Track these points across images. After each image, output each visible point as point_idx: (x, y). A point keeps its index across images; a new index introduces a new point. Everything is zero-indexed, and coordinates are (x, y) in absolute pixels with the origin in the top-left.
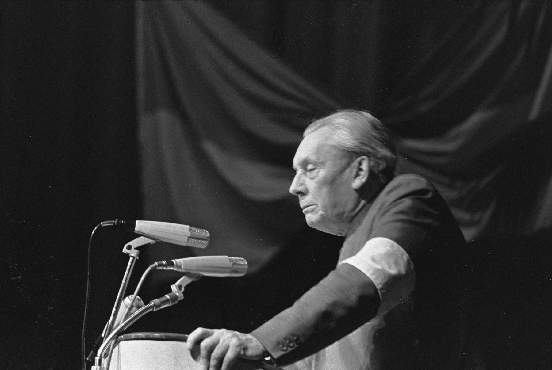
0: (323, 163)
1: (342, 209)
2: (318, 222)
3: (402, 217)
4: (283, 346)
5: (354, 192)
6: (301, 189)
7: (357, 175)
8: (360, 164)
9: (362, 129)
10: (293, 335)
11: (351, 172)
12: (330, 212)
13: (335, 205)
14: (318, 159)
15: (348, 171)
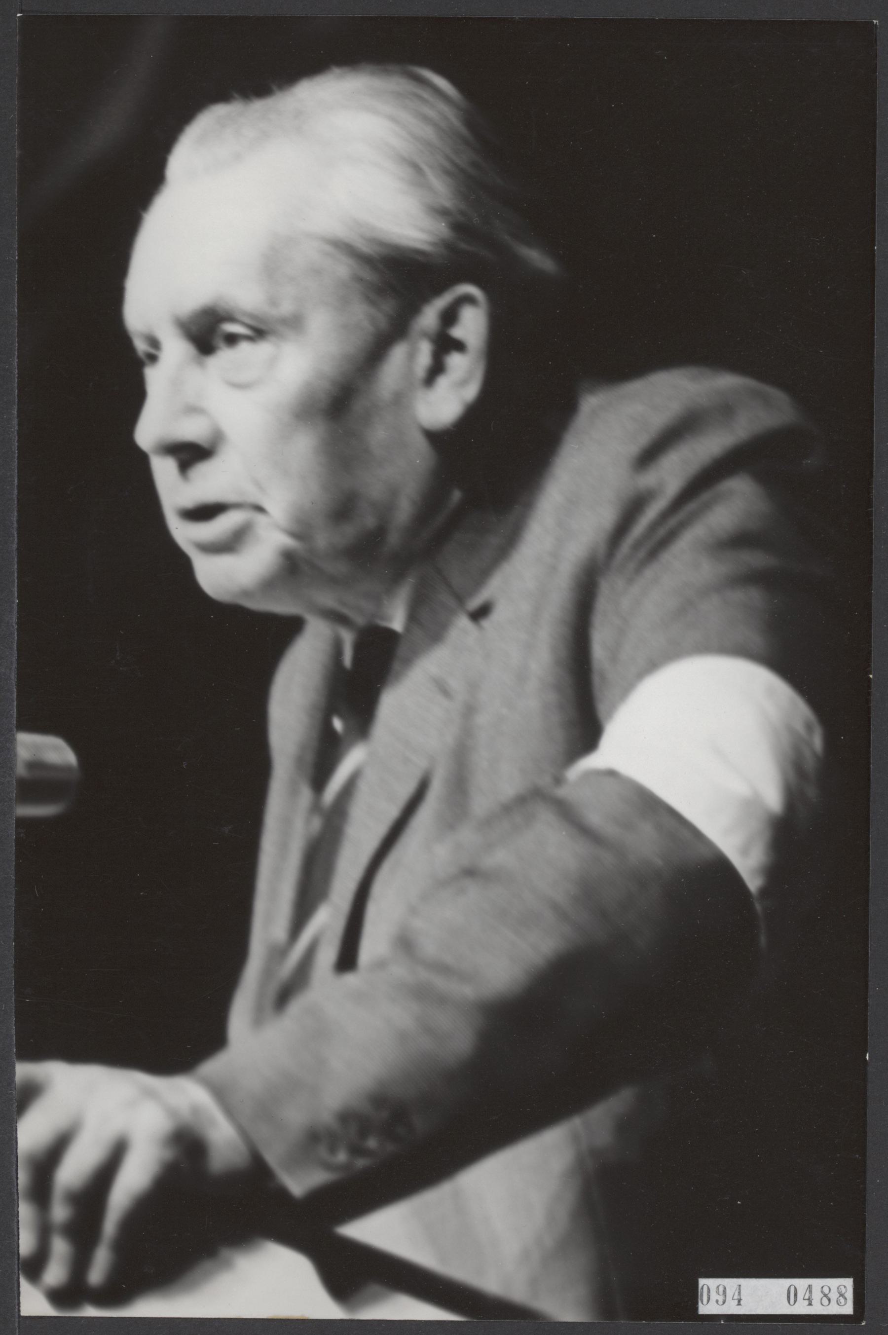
0: (295, 323)
1: (370, 521)
2: (269, 585)
3: (756, 559)
4: (333, 1150)
5: (421, 444)
6: (192, 430)
7: (436, 369)
8: (450, 317)
9: (456, 165)
10: (379, 1099)
11: (411, 356)
12: (322, 540)
13: (343, 509)
14: (273, 302)
15: (398, 354)
